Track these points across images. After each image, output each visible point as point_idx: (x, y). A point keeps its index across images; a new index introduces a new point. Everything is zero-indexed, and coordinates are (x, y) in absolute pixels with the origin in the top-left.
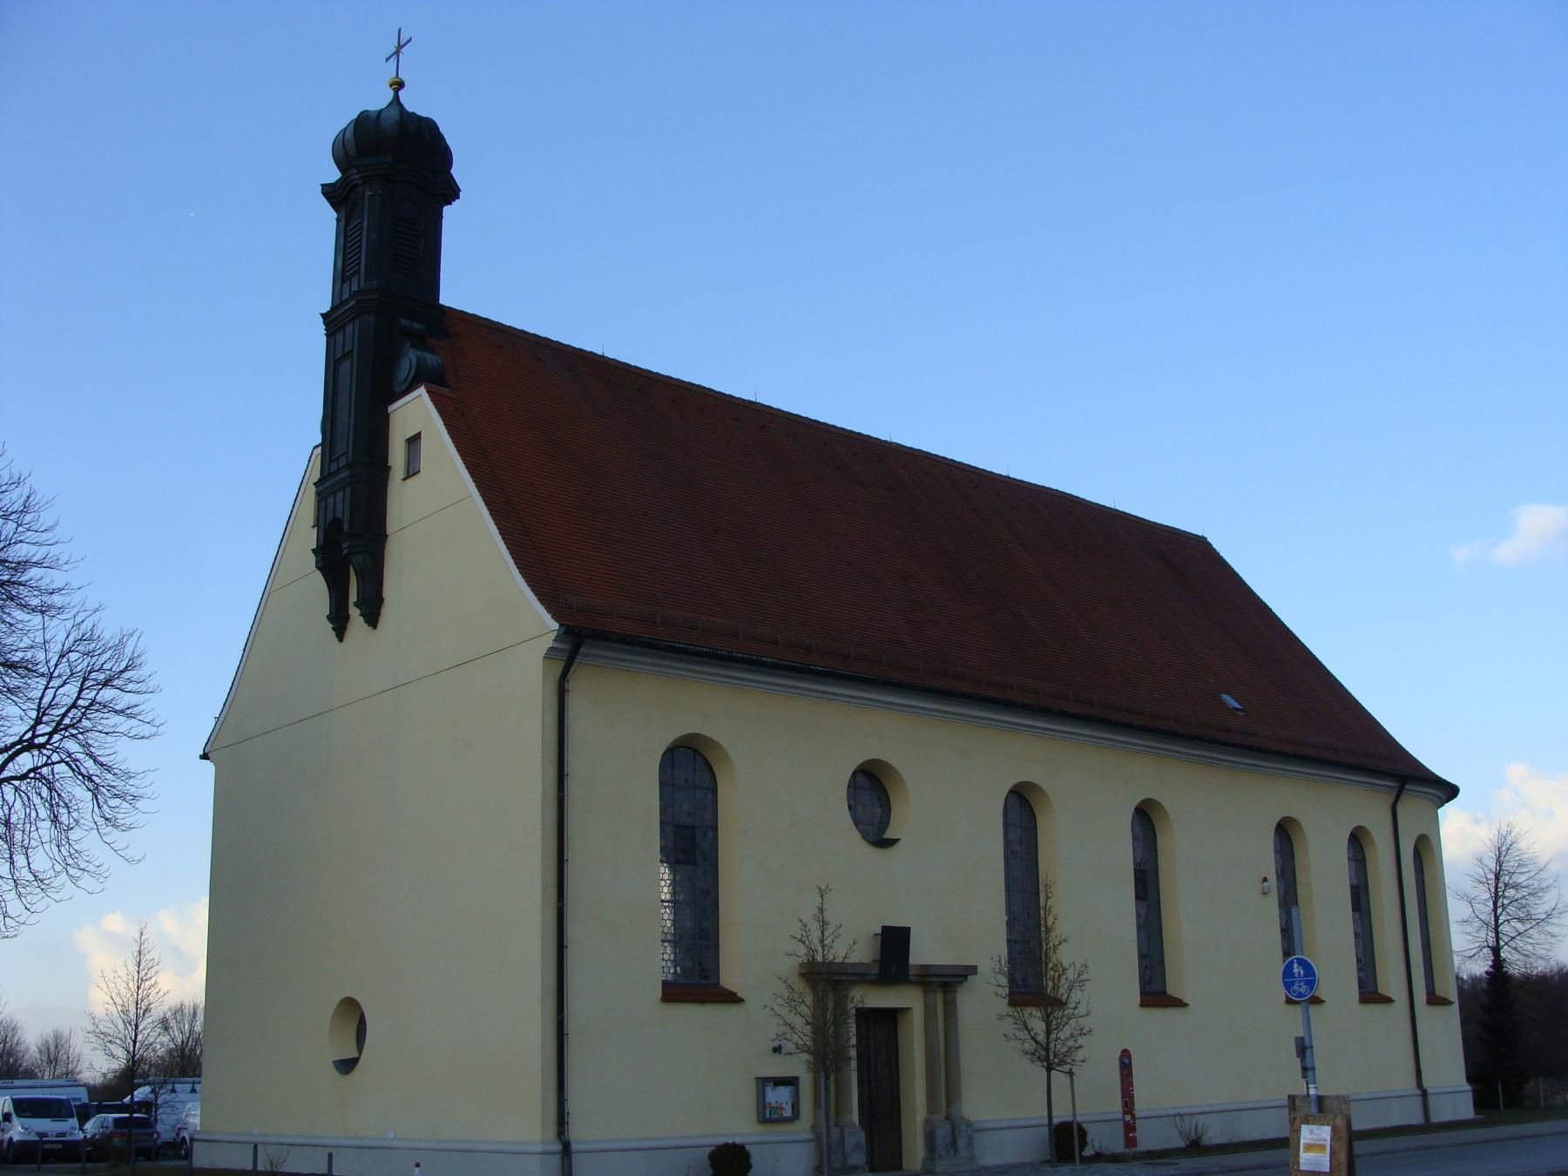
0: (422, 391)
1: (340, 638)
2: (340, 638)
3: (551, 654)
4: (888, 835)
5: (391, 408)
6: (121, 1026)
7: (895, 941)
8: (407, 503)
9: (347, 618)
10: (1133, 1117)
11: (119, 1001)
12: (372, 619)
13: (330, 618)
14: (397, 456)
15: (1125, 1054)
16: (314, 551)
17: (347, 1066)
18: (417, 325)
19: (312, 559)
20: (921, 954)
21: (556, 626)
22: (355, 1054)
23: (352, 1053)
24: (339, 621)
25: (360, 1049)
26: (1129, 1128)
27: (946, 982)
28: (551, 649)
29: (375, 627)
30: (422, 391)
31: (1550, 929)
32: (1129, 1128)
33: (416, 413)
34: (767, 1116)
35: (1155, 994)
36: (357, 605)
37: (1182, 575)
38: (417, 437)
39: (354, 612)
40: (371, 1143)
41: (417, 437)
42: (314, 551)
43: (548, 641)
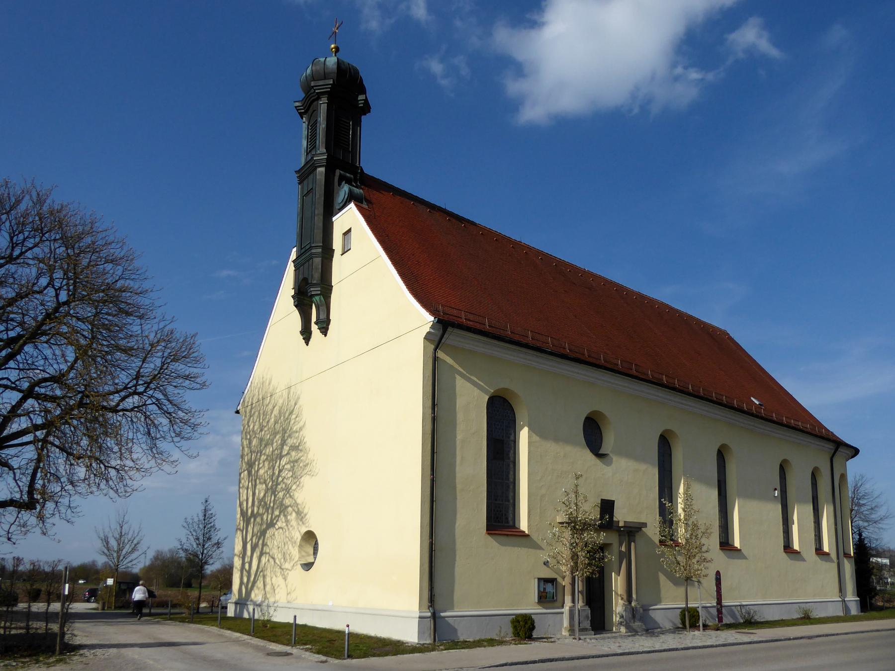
0: (352, 205)
1: (307, 344)
2: (307, 344)
3: (428, 338)
4: (601, 452)
5: (334, 219)
6: (195, 546)
7: (607, 507)
8: (342, 268)
9: (310, 333)
10: (722, 606)
11: (194, 534)
12: (324, 330)
13: (302, 333)
14: (337, 243)
15: (718, 573)
16: (293, 297)
17: (308, 566)
18: (348, 175)
19: (292, 301)
20: (622, 516)
21: (432, 318)
22: (312, 560)
23: (311, 560)
24: (306, 334)
25: (315, 558)
26: (720, 612)
27: (632, 532)
28: (428, 333)
29: (326, 335)
30: (352, 205)
31: (880, 525)
32: (720, 612)
33: (350, 219)
34: (544, 598)
35: (726, 544)
36: (316, 323)
37: (720, 344)
38: (349, 231)
39: (314, 328)
40: (320, 608)
41: (349, 231)
42: (293, 297)
43: (427, 329)
